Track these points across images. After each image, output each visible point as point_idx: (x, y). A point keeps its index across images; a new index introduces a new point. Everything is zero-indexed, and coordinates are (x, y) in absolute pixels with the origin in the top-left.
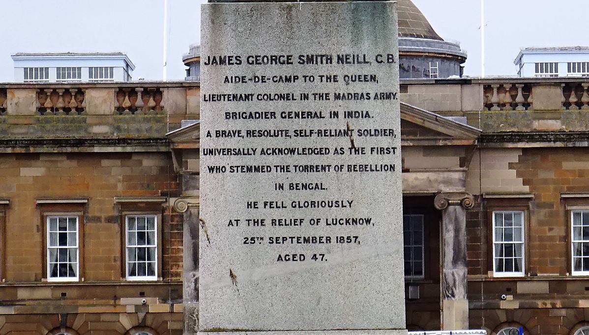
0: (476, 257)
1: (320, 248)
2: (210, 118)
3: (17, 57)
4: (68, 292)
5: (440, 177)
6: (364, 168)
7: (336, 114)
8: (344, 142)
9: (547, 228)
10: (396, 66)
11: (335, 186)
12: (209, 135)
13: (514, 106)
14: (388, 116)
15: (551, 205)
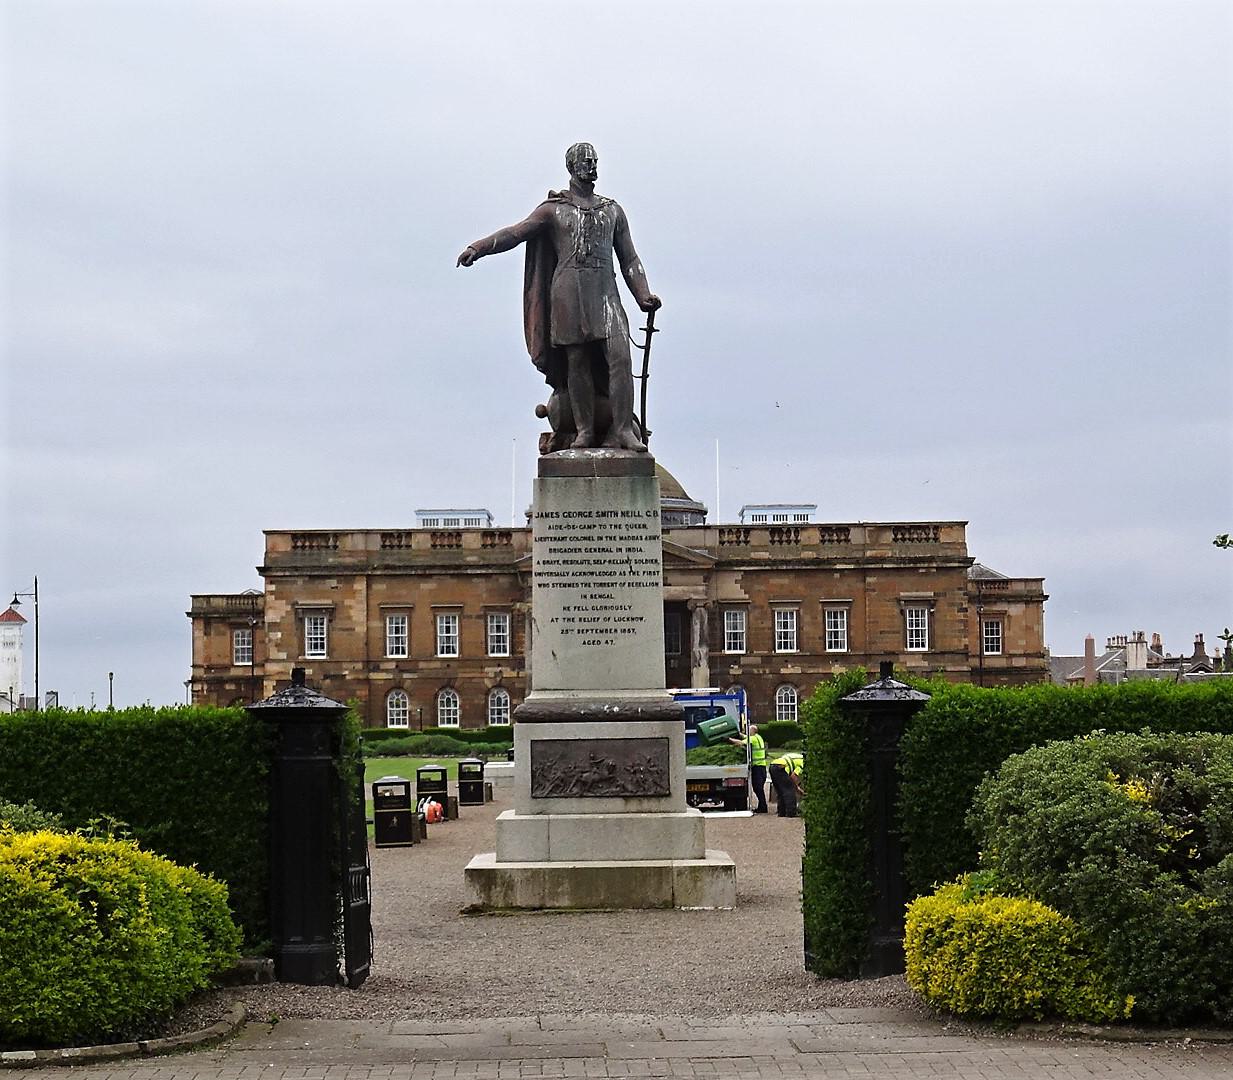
0: (714, 640)
1: (610, 636)
2: (539, 553)
3: (419, 512)
4: (452, 664)
5: (689, 589)
6: (639, 584)
7: (621, 550)
8: (626, 568)
9: (760, 621)
10: (659, 518)
11: (620, 596)
12: (538, 563)
13: (738, 543)
14: (655, 551)
15: (762, 607)
